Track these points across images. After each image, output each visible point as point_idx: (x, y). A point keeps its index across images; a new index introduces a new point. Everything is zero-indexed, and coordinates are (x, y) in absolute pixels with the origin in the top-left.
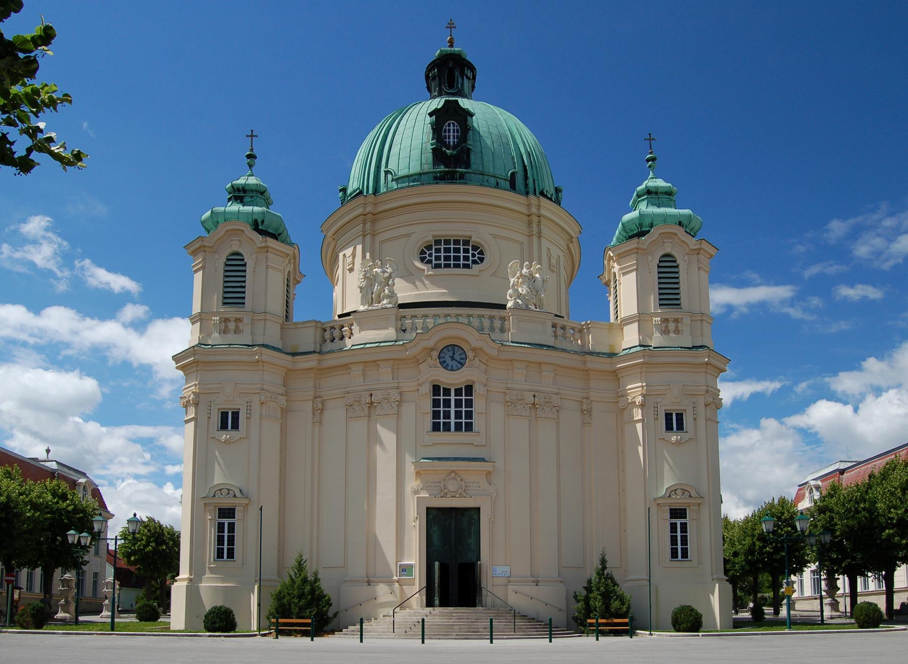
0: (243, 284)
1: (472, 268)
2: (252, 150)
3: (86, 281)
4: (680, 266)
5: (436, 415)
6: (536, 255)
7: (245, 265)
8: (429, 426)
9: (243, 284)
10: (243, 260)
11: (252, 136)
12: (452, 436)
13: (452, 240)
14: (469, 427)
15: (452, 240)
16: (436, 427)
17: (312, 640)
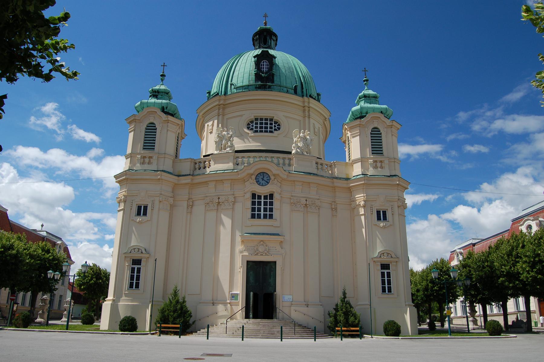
5: (253, 209)
8: (249, 215)
12: (262, 221)
14: (271, 216)
16: (253, 216)
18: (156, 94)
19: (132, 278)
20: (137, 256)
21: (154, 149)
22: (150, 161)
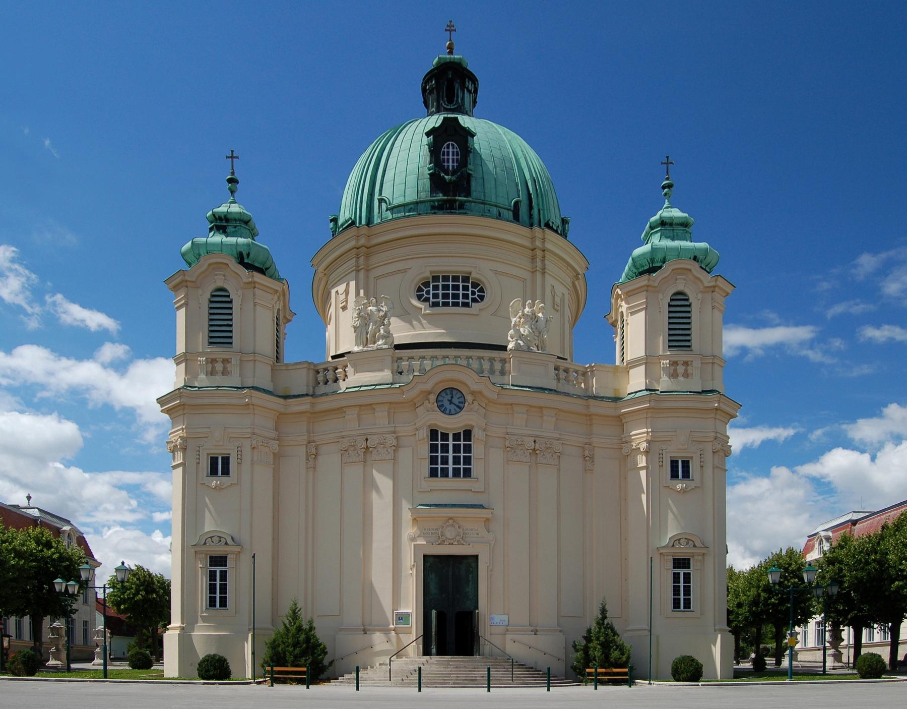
5: (433, 460)
8: (427, 472)
12: (450, 482)
14: (467, 473)
16: (433, 473)
18: (222, 224)
19: (212, 589)
20: (219, 550)
21: (231, 343)
22: (225, 368)
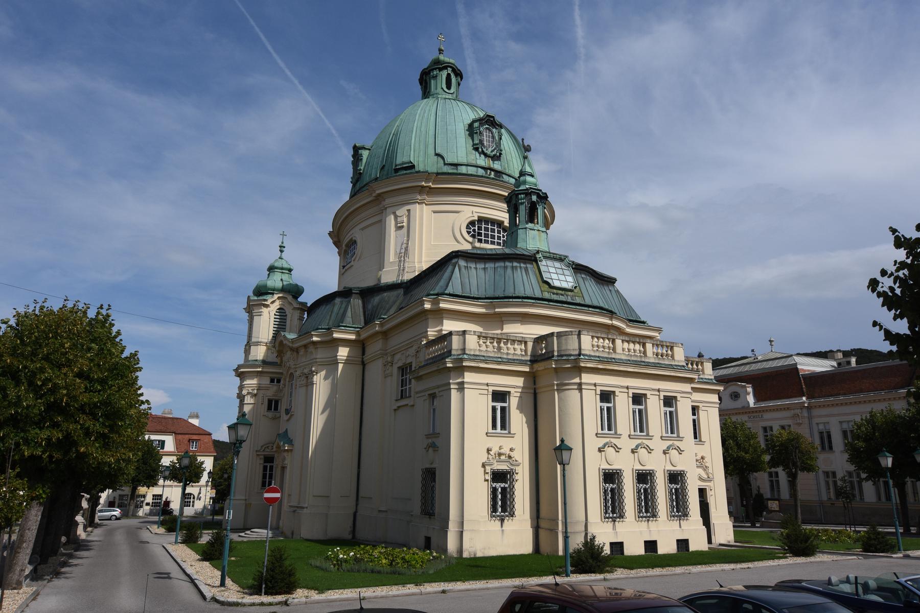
0: (285, 318)
1: (410, 396)
2: (282, 243)
3: (578, 552)
4: (288, 316)
6: (281, 324)
7: (286, 315)
9: (285, 318)
10: (285, 313)
11: (283, 235)
13: (273, 409)
15: (273, 409)
17: (158, 528)
